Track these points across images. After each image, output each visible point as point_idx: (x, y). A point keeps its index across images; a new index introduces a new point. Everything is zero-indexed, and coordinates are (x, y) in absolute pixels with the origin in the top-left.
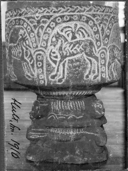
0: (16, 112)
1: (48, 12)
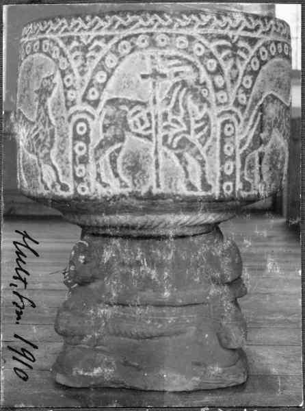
1: (82, 28)
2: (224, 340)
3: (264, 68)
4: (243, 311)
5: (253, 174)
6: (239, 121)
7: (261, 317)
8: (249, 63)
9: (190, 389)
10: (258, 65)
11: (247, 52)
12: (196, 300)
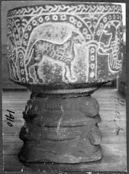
0: (14, 113)
2: (92, 141)
3: (34, 29)
4: (100, 128)
5: (34, 75)
6: (24, 52)
7: (108, 131)
8: (27, 28)
9: (78, 162)
10: (31, 28)
11: (25, 23)
12: (80, 124)
